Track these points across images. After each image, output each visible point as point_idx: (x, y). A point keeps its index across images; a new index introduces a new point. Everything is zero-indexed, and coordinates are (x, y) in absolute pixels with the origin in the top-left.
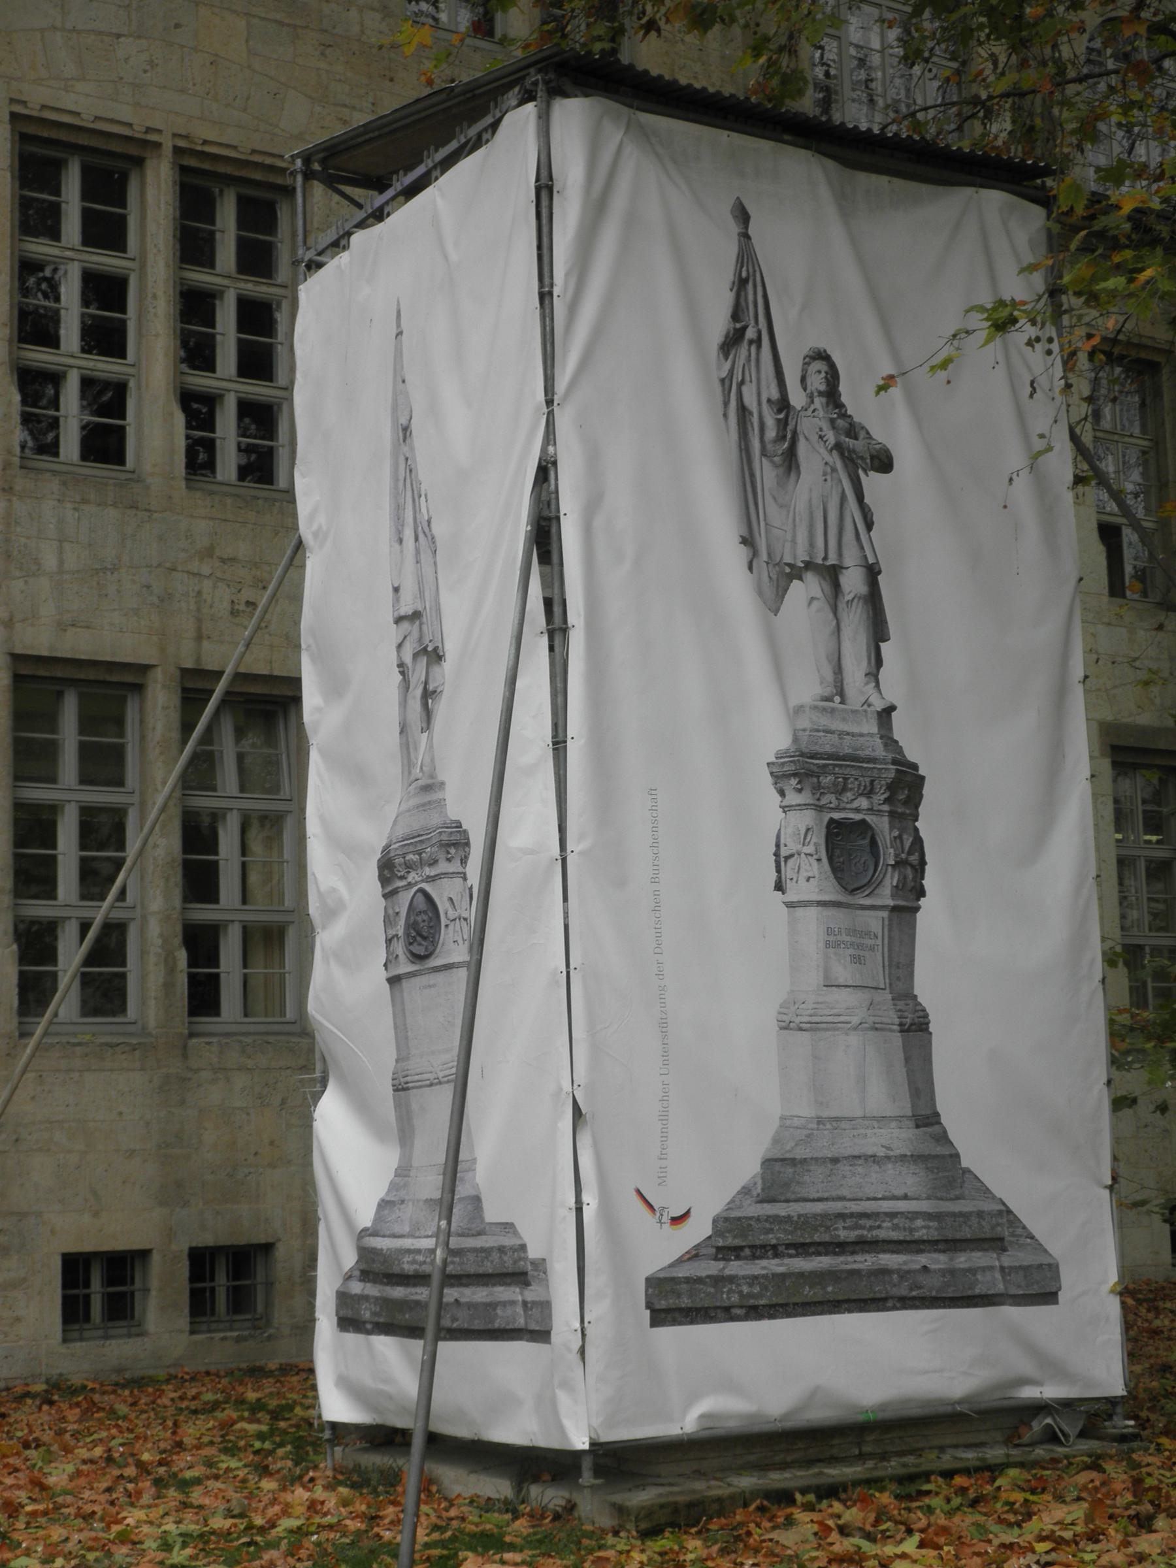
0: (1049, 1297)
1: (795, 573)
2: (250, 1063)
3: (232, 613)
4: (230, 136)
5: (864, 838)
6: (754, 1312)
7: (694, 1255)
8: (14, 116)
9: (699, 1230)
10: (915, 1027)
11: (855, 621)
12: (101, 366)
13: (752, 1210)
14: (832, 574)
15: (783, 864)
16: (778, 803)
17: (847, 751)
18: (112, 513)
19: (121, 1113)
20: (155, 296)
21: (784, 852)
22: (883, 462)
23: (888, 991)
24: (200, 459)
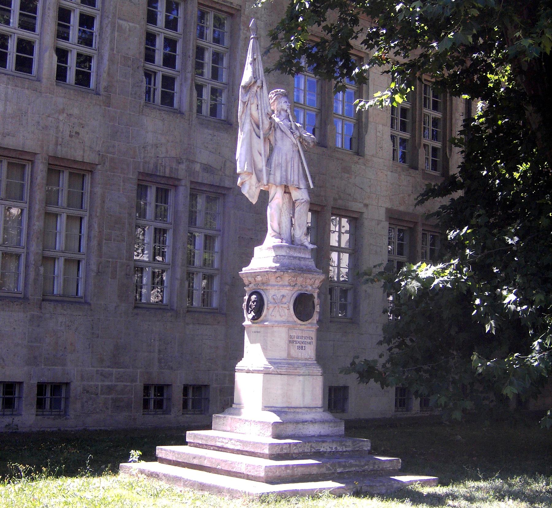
2: (65, 313)
3: (70, 136)
12: (89, 9)
19: (14, 329)
20: (49, 9)
24: (61, 74)
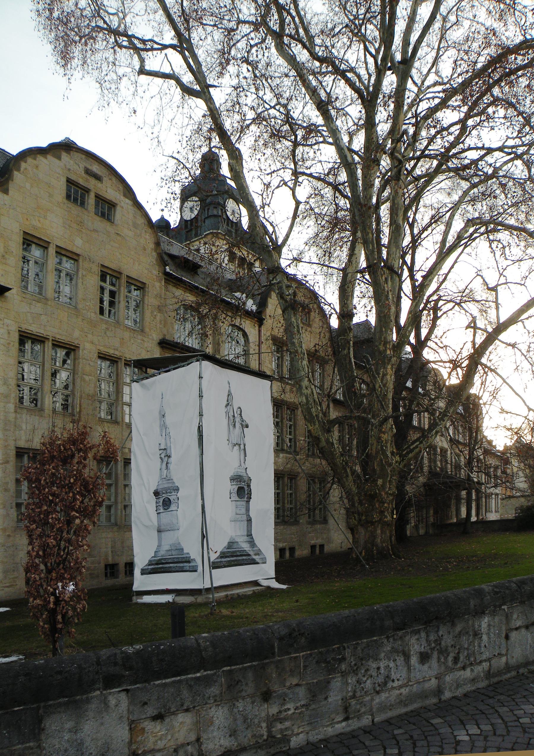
0: (265, 563)
1: (235, 445)
4: (63, 338)
6: (225, 567)
7: (217, 558)
8: (19, 331)
9: (218, 554)
10: (249, 520)
11: (242, 452)
13: (226, 550)
14: (240, 445)
18: (37, 417)
22: (247, 426)
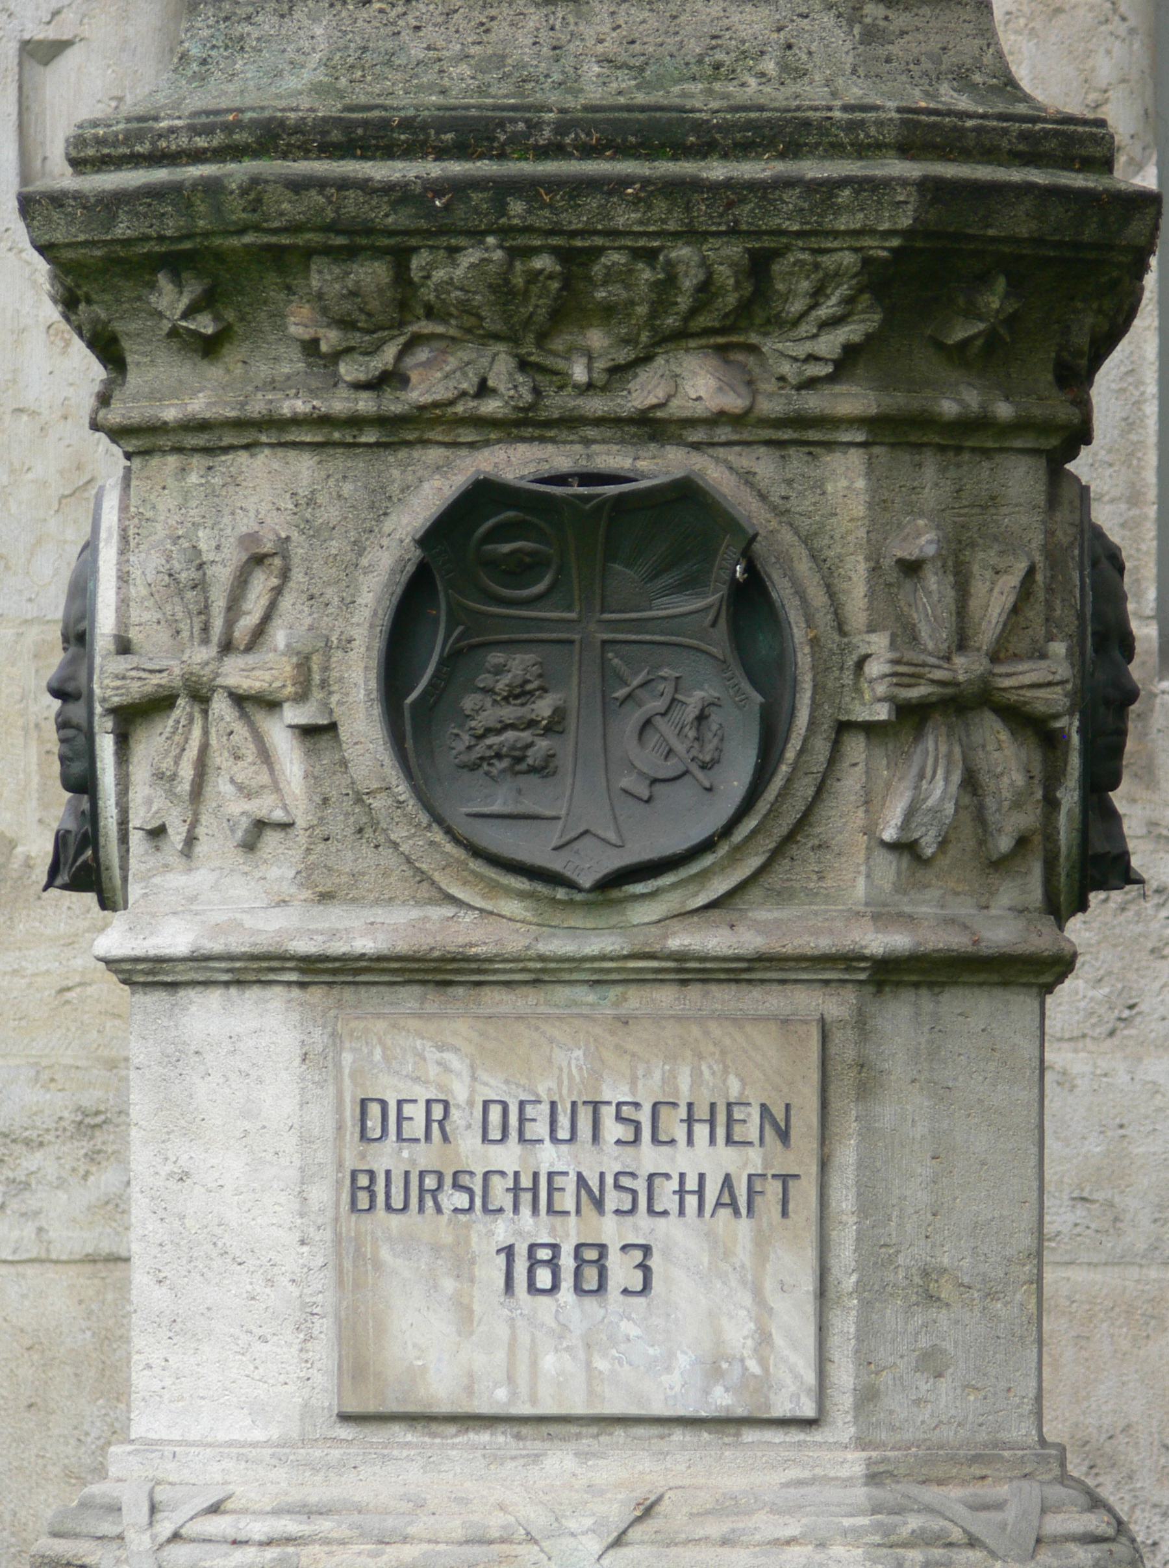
5: (691, 584)
15: (106, 746)
16: (86, 402)
17: (597, 87)
21: (111, 680)
23: (842, 1427)
